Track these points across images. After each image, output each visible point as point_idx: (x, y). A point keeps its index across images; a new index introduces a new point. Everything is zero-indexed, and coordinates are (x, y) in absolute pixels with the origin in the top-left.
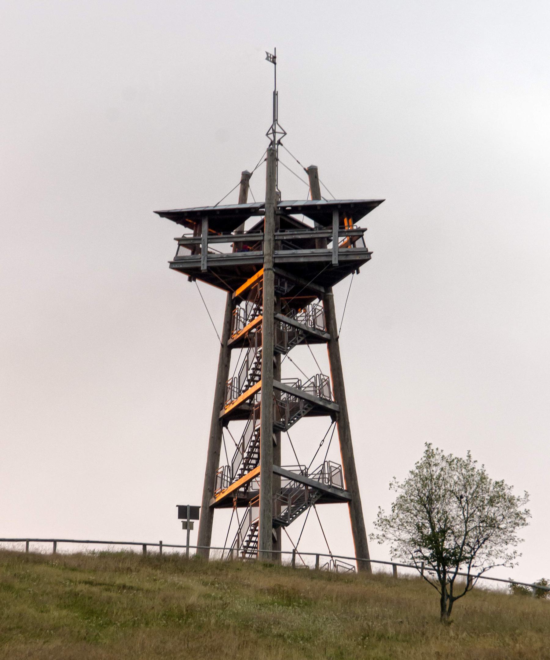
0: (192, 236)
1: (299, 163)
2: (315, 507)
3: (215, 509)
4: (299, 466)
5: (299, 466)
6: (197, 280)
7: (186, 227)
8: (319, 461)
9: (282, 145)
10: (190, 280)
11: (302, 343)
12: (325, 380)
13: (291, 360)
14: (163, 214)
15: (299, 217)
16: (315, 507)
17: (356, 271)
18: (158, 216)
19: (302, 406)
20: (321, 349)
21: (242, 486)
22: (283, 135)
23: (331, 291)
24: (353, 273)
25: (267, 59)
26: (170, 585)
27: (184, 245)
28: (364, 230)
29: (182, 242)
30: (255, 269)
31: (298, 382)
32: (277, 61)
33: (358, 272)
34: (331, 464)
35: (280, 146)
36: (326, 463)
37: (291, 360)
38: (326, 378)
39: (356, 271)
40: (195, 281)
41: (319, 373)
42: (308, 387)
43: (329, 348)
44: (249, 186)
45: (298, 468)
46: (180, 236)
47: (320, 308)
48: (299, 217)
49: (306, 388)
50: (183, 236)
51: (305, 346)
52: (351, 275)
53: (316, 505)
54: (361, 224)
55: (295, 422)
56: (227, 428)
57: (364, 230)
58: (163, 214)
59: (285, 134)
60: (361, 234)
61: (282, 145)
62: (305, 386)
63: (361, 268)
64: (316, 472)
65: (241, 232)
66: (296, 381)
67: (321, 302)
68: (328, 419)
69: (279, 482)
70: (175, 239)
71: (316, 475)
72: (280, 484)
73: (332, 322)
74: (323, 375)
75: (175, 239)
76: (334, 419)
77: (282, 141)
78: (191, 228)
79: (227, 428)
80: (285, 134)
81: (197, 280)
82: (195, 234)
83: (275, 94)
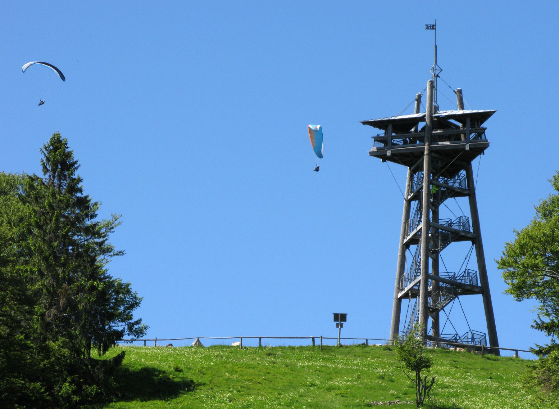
0: (383, 135)
1: (450, 87)
2: (458, 298)
3: (402, 300)
4: (448, 273)
5: (448, 273)
6: (387, 161)
7: (380, 129)
8: (463, 270)
9: (439, 77)
10: (383, 161)
11: (452, 197)
12: (467, 220)
13: (447, 207)
14: (364, 123)
15: (452, 121)
16: (458, 298)
17: (482, 153)
18: (362, 124)
19: (450, 235)
20: (464, 201)
21: (415, 285)
22: (440, 71)
23: (470, 164)
24: (481, 154)
25: (427, 28)
26: (54, 319)
27: (377, 141)
28: (485, 129)
29: (378, 139)
30: (468, 121)
31: (450, 221)
32: (437, 27)
33: (483, 154)
34: (469, 271)
35: (438, 78)
36: (466, 271)
37: (447, 207)
38: (467, 218)
39: (482, 153)
40: (386, 162)
41: (462, 215)
42: (456, 223)
43: (469, 199)
44: (421, 102)
45: (447, 274)
46: (375, 135)
47: (463, 175)
48: (452, 121)
49: (454, 224)
50: (377, 135)
51: (453, 199)
52: (479, 156)
53: (460, 297)
54: (484, 125)
55: (448, 244)
56: (409, 250)
57: (485, 129)
58: (364, 123)
59: (441, 70)
60: (483, 131)
61: (439, 77)
62: (454, 223)
63: (485, 151)
64: (461, 276)
65: (416, 130)
66: (448, 220)
67: (465, 171)
68: (469, 243)
69: (439, 283)
70: (373, 137)
71: (461, 277)
72: (439, 285)
73: (471, 183)
74: (465, 217)
75: (373, 137)
76: (473, 243)
77: (439, 75)
78: (383, 129)
79: (409, 250)
80: (441, 70)
81: (387, 161)
82: (385, 134)
83: (436, 47)
